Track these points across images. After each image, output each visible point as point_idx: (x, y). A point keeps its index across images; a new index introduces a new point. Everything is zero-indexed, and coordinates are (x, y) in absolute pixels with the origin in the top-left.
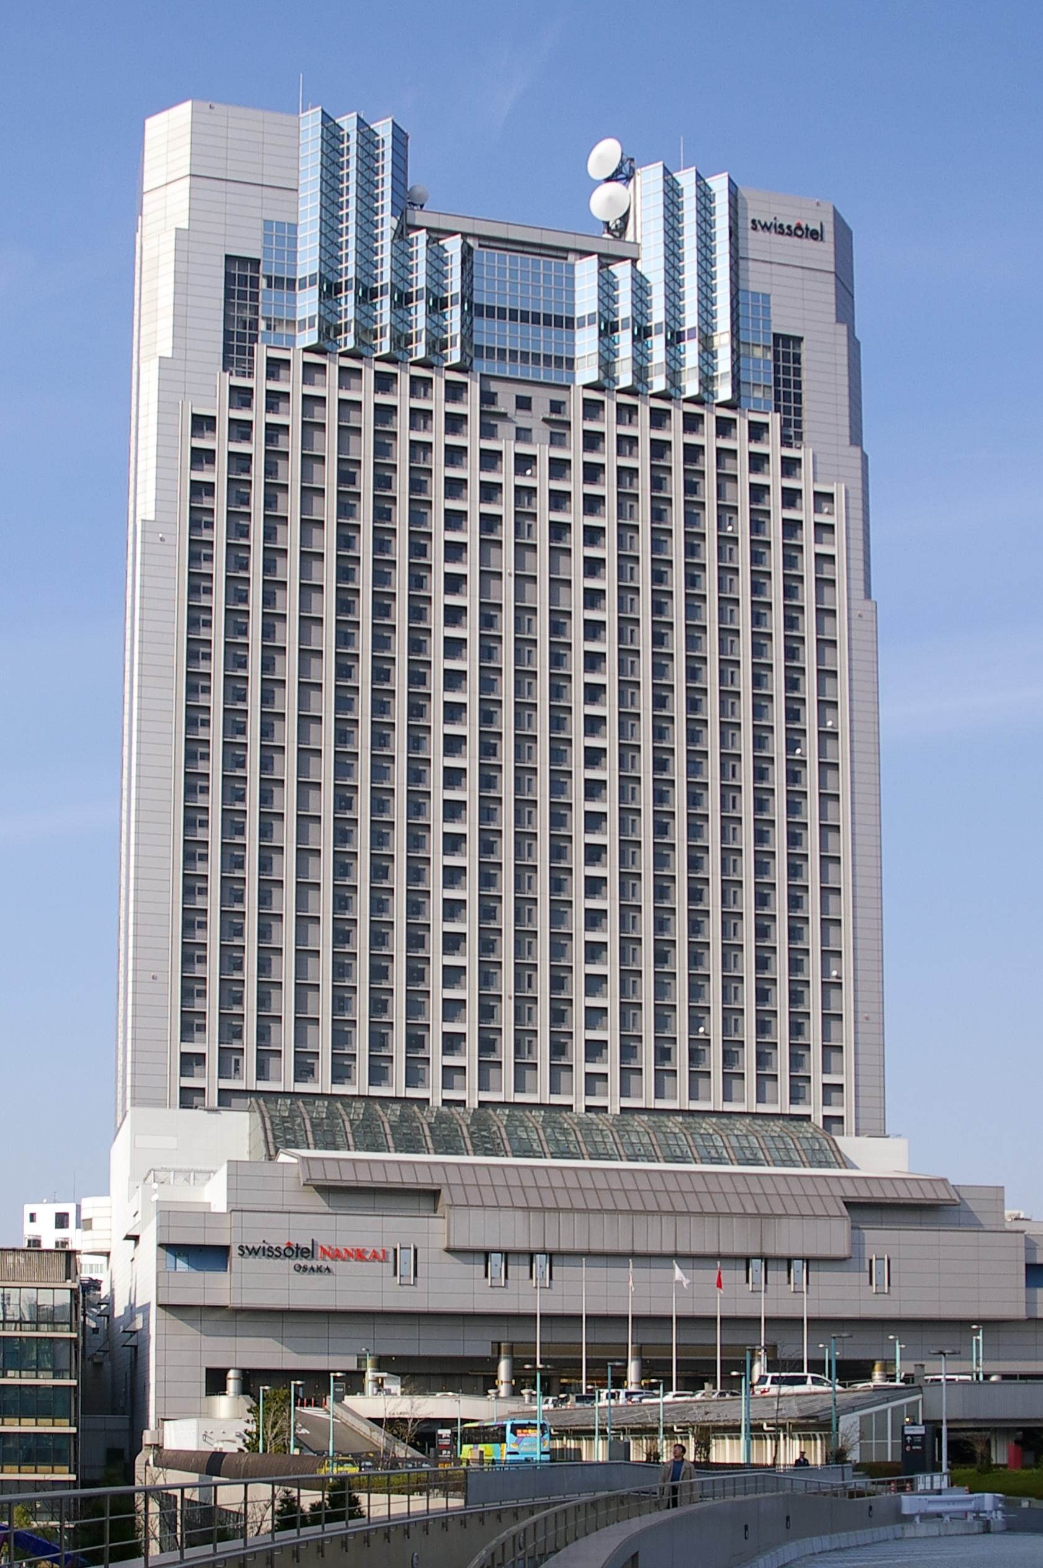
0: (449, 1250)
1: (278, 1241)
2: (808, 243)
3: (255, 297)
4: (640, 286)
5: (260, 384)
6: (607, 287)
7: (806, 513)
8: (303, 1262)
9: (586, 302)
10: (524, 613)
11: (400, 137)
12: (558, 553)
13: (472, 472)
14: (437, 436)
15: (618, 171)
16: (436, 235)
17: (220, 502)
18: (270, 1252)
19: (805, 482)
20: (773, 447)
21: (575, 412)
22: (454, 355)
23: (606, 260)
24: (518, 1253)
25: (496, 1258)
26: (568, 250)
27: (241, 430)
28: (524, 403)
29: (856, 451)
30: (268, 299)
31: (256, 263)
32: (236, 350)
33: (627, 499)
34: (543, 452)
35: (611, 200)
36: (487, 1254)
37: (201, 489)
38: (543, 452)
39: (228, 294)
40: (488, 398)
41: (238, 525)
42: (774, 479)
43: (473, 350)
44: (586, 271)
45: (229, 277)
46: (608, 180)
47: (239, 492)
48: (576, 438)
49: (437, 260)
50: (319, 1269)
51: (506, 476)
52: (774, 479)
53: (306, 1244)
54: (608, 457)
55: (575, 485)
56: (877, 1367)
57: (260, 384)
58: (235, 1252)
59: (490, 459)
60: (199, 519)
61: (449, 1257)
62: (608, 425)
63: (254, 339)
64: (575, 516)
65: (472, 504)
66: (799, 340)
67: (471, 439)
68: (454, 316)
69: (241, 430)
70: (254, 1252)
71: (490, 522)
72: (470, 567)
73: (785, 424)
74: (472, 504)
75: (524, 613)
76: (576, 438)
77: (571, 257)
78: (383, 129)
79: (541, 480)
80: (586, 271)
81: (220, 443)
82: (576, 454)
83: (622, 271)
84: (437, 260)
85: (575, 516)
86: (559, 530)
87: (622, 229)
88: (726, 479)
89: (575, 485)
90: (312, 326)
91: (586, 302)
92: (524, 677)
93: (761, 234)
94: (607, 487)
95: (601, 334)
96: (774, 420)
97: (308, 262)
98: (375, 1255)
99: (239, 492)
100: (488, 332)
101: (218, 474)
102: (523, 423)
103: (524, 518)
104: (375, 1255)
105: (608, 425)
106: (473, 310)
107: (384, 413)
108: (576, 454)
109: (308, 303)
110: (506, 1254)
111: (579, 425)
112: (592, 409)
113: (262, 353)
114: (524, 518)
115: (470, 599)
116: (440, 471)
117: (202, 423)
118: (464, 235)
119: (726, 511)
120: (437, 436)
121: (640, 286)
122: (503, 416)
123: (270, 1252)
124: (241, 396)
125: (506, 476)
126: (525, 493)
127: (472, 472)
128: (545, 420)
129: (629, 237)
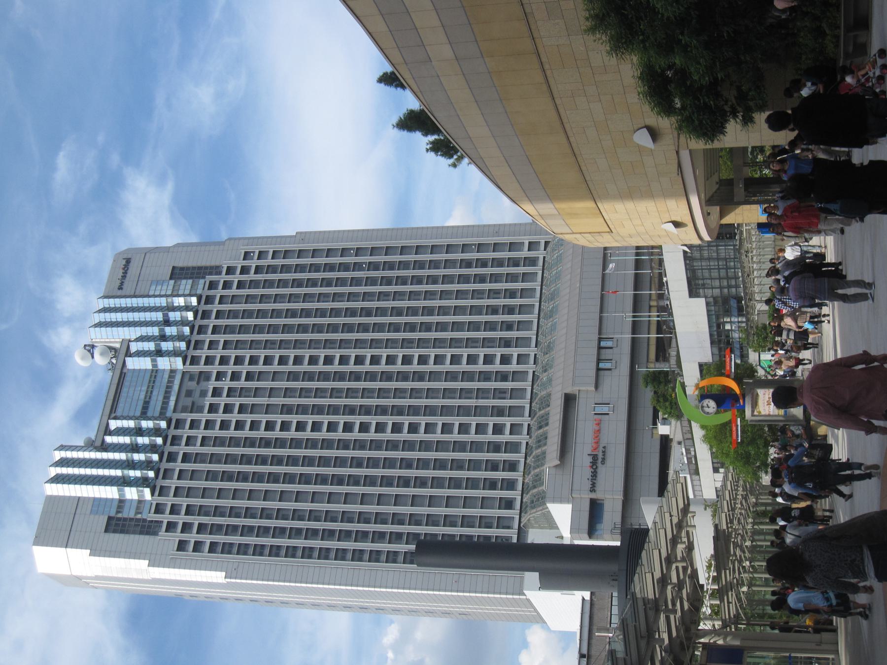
0: (597, 387)
1: (588, 472)
2: (131, 264)
3: (125, 519)
4: (141, 339)
5: (166, 518)
6: (140, 354)
7: (253, 263)
8: (600, 460)
9: (145, 363)
10: (288, 392)
11: (62, 448)
12: (261, 376)
13: (219, 417)
14: (200, 433)
15: (89, 351)
16: (108, 432)
17: (220, 538)
18: (594, 475)
19: (239, 263)
20: (223, 278)
21: (195, 369)
22: (163, 424)
23: (128, 354)
24: (599, 354)
25: (601, 365)
26: (121, 373)
27: (186, 527)
28: (189, 393)
29: (227, 243)
30: (129, 513)
31: (110, 518)
32: (148, 528)
33: (238, 345)
34: (212, 384)
35: (102, 354)
36: (598, 369)
37: (213, 548)
38: (212, 384)
39: (122, 532)
40: (184, 410)
41: (232, 530)
42: (236, 278)
43: (162, 416)
44: (133, 363)
45: (115, 531)
46: (93, 357)
47: (216, 529)
48: (208, 368)
49: (120, 432)
50: (604, 452)
51: (222, 401)
52: (236, 278)
53: (590, 459)
54: (218, 353)
55: (230, 368)
56: (436, 137)
57: (166, 518)
58: (593, 496)
59: (213, 408)
60: (227, 549)
61: (600, 388)
62: (203, 353)
63: (144, 520)
64: (244, 369)
65: (234, 417)
66: (174, 268)
67: (204, 417)
68: (146, 424)
69: (186, 527)
70: (593, 485)
71: (242, 409)
72: (263, 418)
73: (210, 274)
74: (234, 417)
75: (288, 392)
76: (208, 368)
77: (125, 371)
78: (58, 455)
79: (226, 384)
80: (133, 363)
81: (192, 537)
82: (214, 369)
83: (134, 347)
84: (120, 432)
85: (244, 369)
86: (249, 377)
87: (115, 349)
88: (234, 299)
89: (230, 368)
90: (142, 491)
91: (145, 363)
92: (277, 298)
93: (125, 286)
94: (233, 354)
95: (161, 356)
96: (209, 278)
97: (110, 492)
98: (598, 424)
99: (216, 529)
100: (156, 406)
101: (207, 539)
102: (197, 393)
103: (243, 392)
104: (598, 424)
105: (203, 353)
106: (144, 415)
107: (186, 458)
108: (214, 369)
109: (131, 493)
110: (599, 360)
111: (201, 367)
112: (194, 361)
113: (153, 517)
114: (243, 392)
115: (279, 419)
116: (216, 432)
117: (182, 546)
118: (109, 418)
119: (249, 299)
120: (200, 433)
121: (141, 339)
122: (193, 403)
123: (594, 475)
124: (171, 526)
125: (222, 401)
126: (231, 392)
127: (219, 417)
128: (198, 383)
129: (118, 346)
